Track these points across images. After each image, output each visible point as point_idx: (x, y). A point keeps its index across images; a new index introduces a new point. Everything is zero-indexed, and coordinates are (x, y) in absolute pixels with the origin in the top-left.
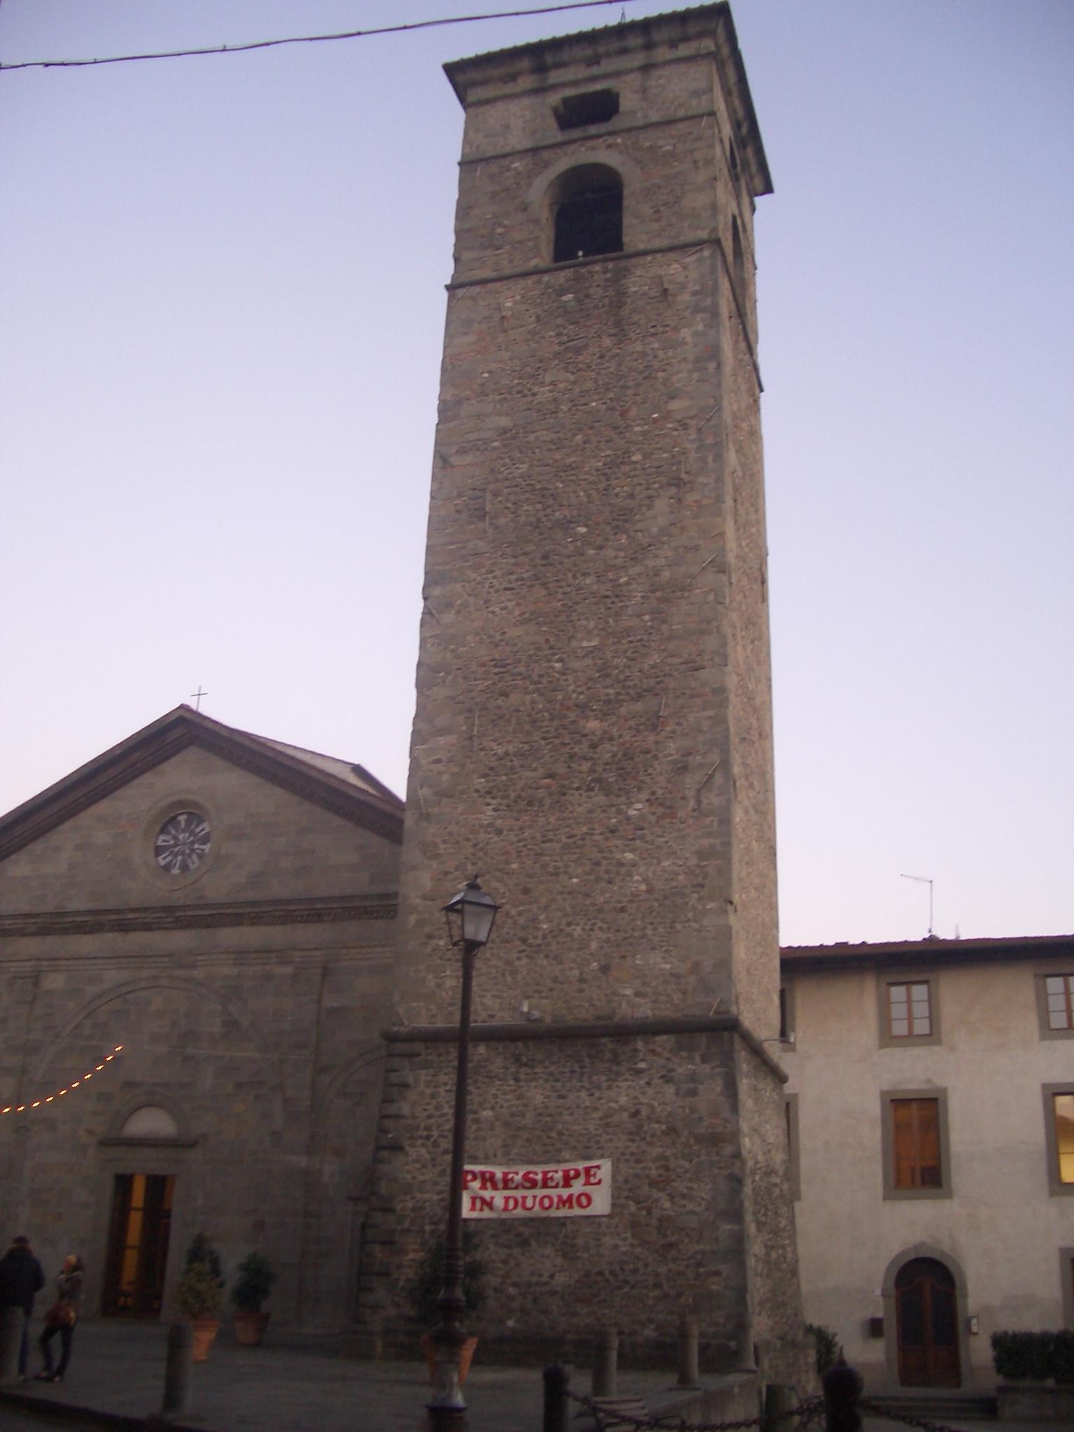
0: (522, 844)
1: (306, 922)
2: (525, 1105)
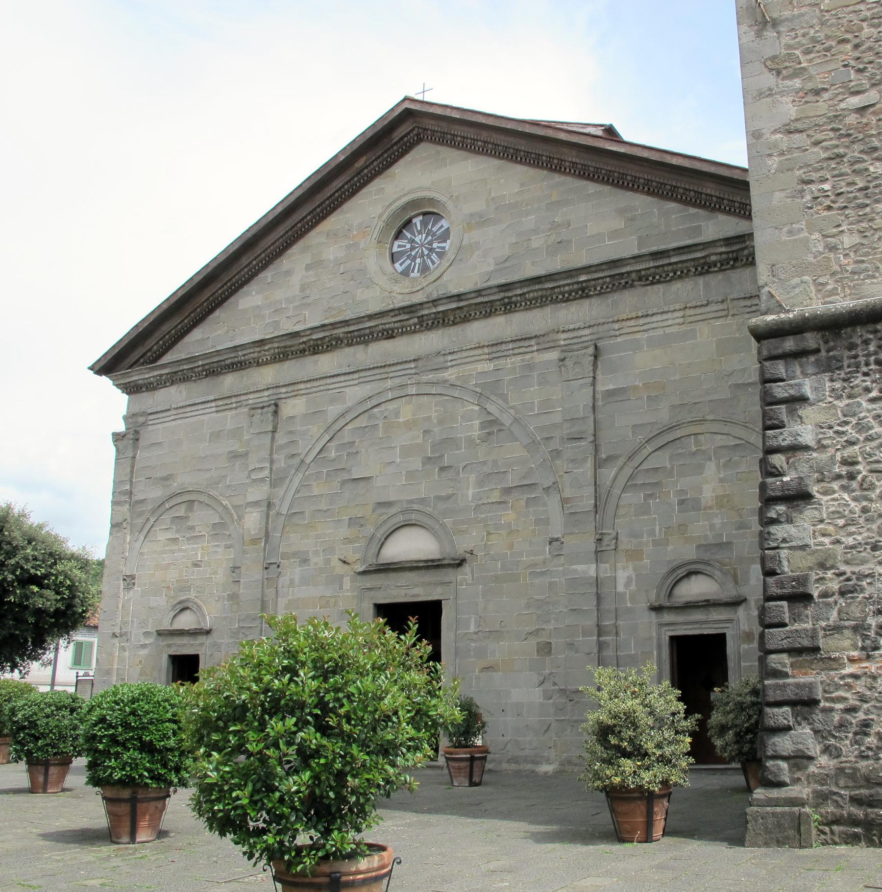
1: (568, 300)
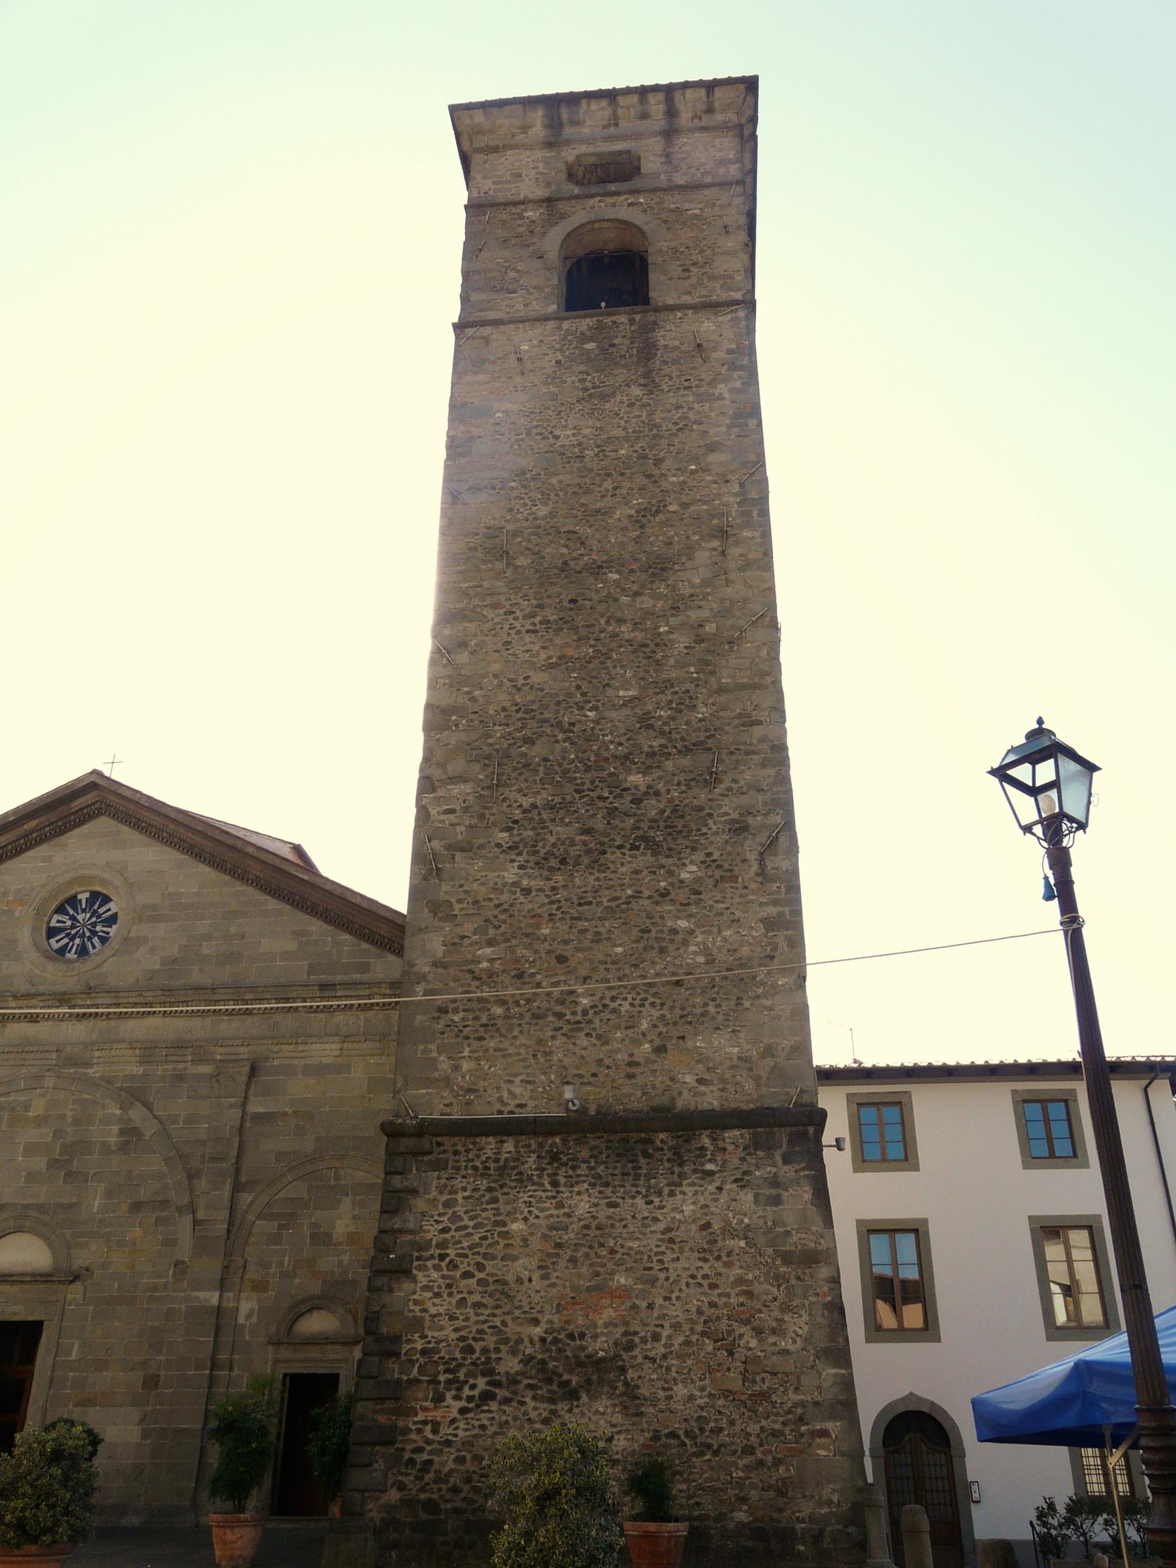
0: (555, 906)
2: (568, 1215)
